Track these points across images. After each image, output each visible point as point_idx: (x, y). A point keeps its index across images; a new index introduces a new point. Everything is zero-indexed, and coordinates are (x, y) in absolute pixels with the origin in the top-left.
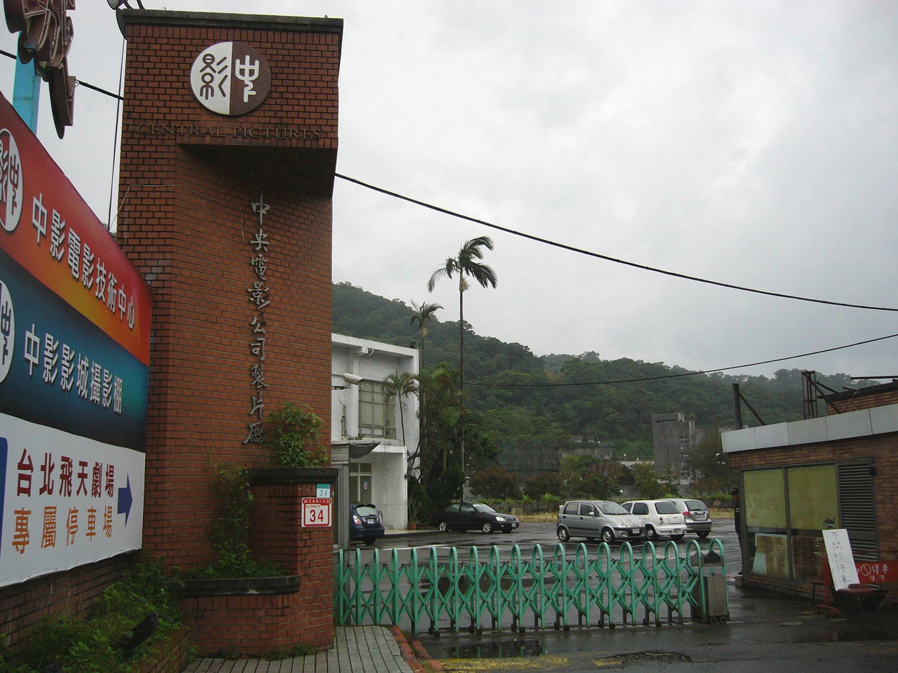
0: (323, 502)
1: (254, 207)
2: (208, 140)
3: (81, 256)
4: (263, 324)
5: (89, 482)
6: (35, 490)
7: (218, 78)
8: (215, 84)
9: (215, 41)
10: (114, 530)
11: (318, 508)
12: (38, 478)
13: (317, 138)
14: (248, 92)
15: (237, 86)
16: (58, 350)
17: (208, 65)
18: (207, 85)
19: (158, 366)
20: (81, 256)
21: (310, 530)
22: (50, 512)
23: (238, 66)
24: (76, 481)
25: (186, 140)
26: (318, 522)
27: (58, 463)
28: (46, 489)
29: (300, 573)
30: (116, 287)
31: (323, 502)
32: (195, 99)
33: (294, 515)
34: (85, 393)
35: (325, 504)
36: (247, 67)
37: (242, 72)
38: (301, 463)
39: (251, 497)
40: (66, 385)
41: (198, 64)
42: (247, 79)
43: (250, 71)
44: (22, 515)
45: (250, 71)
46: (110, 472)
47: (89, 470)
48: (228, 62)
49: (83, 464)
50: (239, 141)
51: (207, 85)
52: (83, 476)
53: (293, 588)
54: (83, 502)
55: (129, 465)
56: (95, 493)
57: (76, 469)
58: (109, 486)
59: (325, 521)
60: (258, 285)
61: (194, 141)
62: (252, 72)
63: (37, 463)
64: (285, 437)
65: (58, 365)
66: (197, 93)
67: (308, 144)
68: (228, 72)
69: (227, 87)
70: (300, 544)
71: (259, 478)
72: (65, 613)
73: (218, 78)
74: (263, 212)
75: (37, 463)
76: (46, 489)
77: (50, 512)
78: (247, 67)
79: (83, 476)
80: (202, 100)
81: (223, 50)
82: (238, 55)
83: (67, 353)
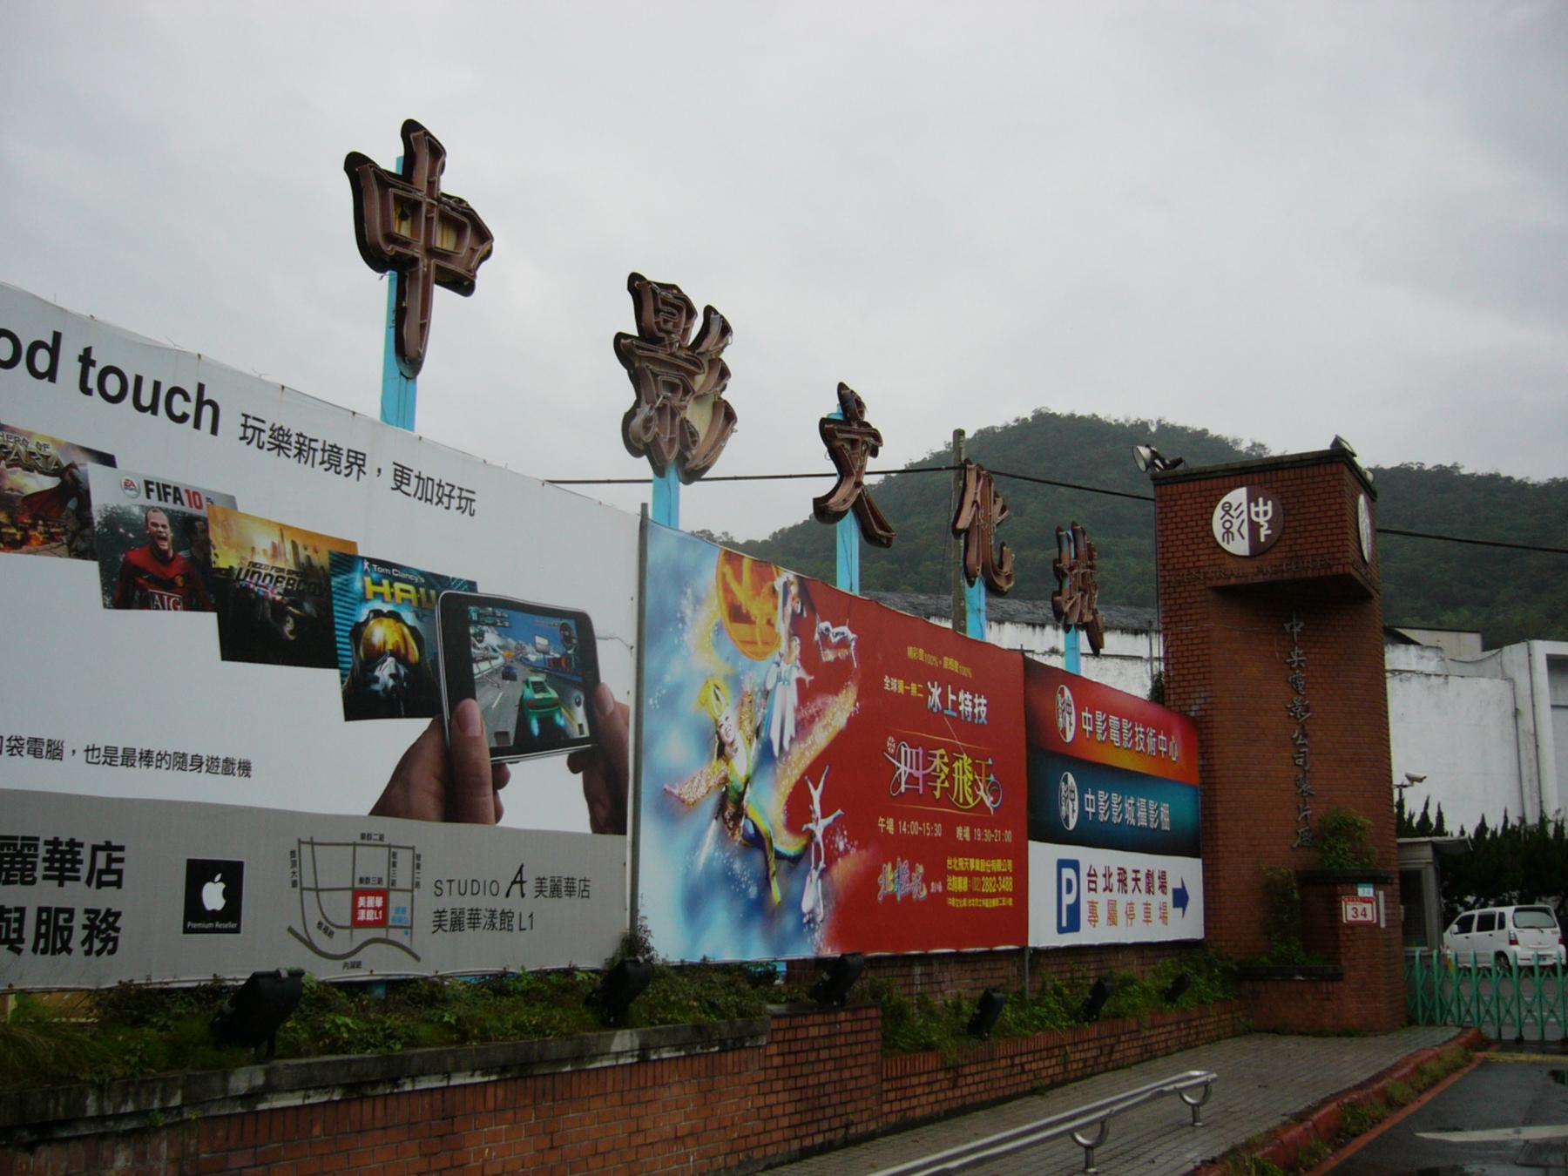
0: (1366, 900)
1: (1287, 626)
2: (1233, 581)
3: (1120, 730)
4: (1305, 736)
5: (1142, 884)
6: (1100, 890)
7: (1236, 523)
8: (1234, 529)
9: (1231, 489)
10: (1169, 916)
11: (1360, 907)
12: (1101, 883)
13: (1330, 566)
14: (1264, 532)
15: (1254, 527)
16: (1109, 798)
17: (1227, 512)
18: (1228, 531)
19: (1206, 781)
20: (1120, 730)
21: (1353, 926)
22: (1112, 904)
23: (1253, 509)
24: (1131, 884)
25: (1214, 583)
26: (1360, 918)
27: (1115, 872)
28: (1108, 889)
29: (1344, 963)
30: (1155, 735)
31: (1366, 900)
32: (1218, 546)
33: (1336, 912)
34: (1133, 822)
35: (395, 855)
36: (1261, 508)
37: (1257, 514)
38: (1341, 865)
39: (1296, 896)
40: (1116, 820)
41: (1218, 512)
42: (1262, 520)
43: (1264, 511)
44: (1092, 904)
45: (1264, 511)
46: (1163, 876)
47: (1142, 876)
48: (1244, 507)
49: (1136, 872)
50: (1260, 578)
51: (1228, 531)
52: (1136, 880)
53: (1338, 977)
54: (1139, 898)
55: (1186, 871)
56: (1149, 891)
57: (1130, 875)
58: (1163, 887)
59: (1369, 918)
60: (1297, 700)
61: (1221, 583)
62: (1266, 513)
63: (1100, 872)
64: (1332, 841)
65: (1110, 808)
66: (1219, 539)
67: (1322, 573)
68: (1245, 516)
69: (1245, 530)
70: (1343, 938)
71: (1308, 879)
72: (1129, 968)
73: (1236, 523)
74: (1297, 630)
75: (1100, 872)
76: (1108, 889)
77: (1112, 904)
78: (1261, 508)
79: (1136, 880)
80: (1224, 545)
81: (1238, 496)
82: (1252, 499)
83: (1116, 798)
